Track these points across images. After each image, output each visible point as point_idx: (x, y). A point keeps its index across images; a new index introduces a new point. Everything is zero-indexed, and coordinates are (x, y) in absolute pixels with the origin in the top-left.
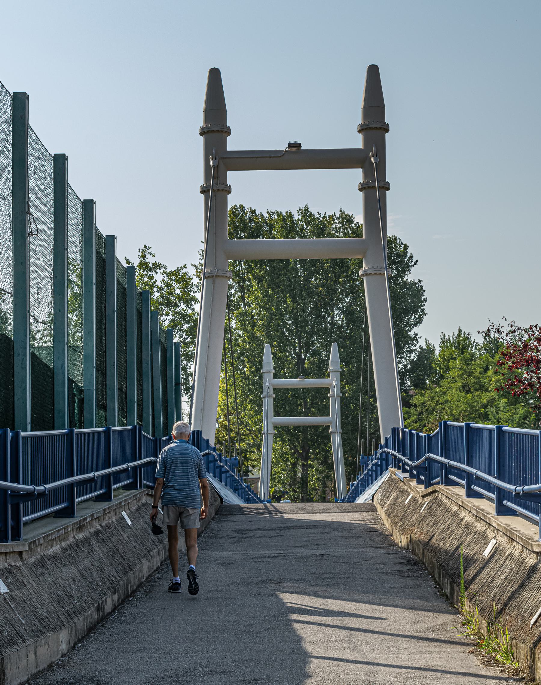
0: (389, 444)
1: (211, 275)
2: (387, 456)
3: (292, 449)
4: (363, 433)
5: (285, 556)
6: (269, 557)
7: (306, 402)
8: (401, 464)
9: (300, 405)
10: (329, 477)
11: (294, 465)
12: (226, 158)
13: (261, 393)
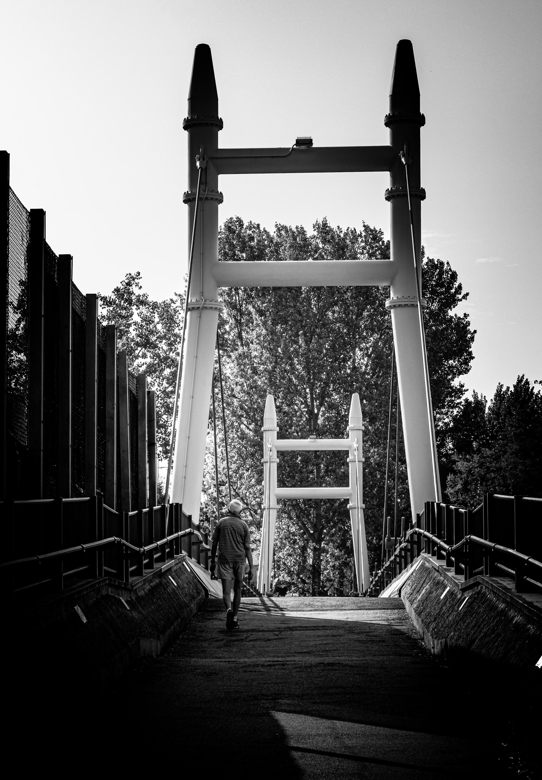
0: (422, 524)
1: (196, 306)
2: (419, 538)
3: (301, 528)
4: (390, 509)
5: (283, 665)
6: (263, 666)
7: (319, 471)
8: (436, 548)
9: (312, 472)
10: (348, 564)
11: (304, 549)
12: (216, 158)
13: (262, 456)
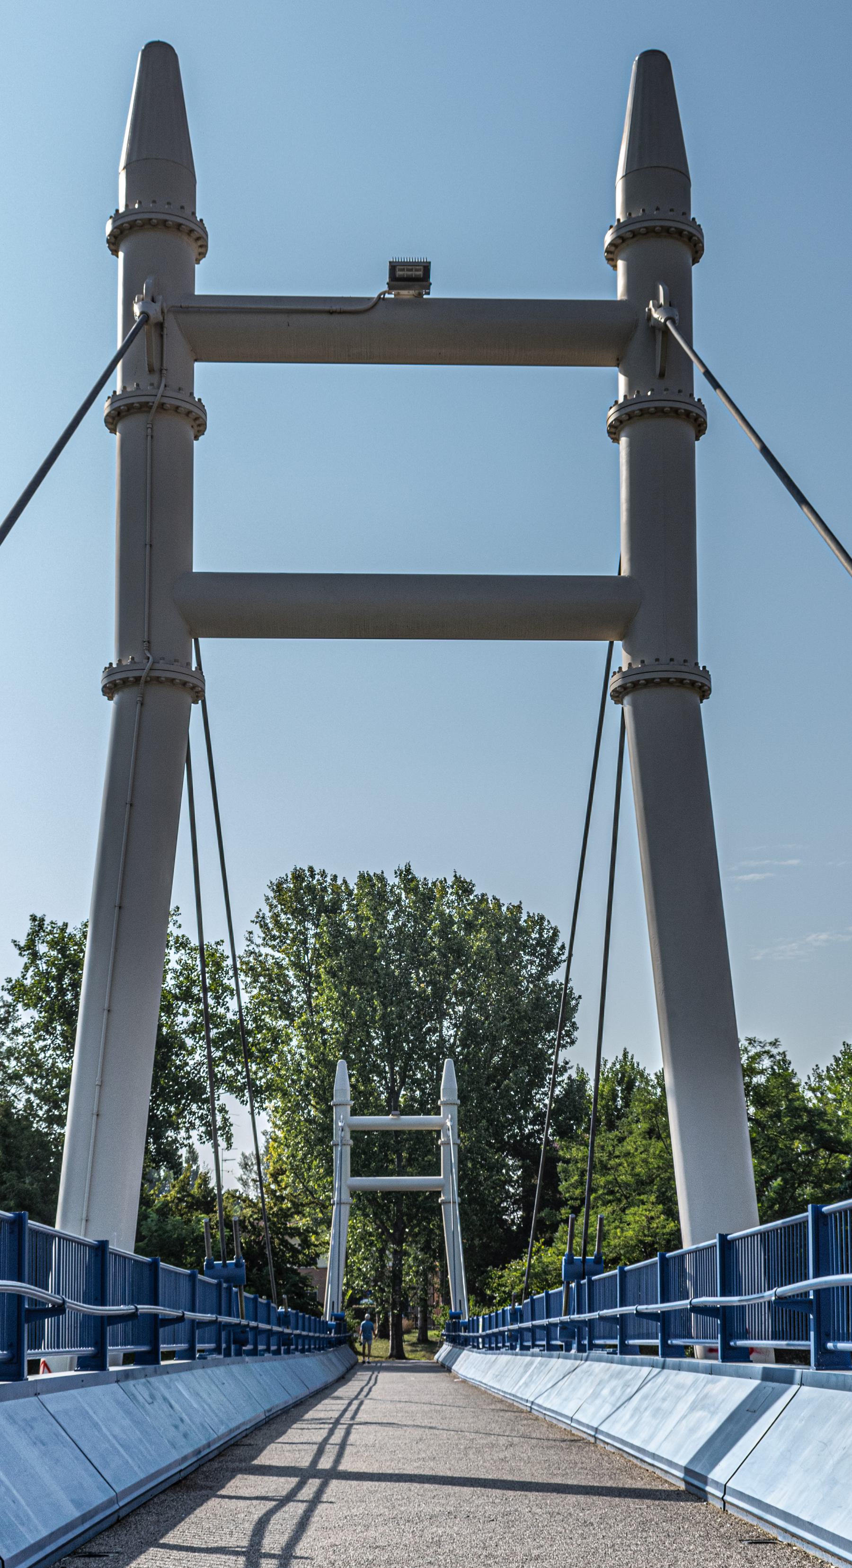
1: (131, 675)
7: (400, 1157)
11: (382, 1251)
